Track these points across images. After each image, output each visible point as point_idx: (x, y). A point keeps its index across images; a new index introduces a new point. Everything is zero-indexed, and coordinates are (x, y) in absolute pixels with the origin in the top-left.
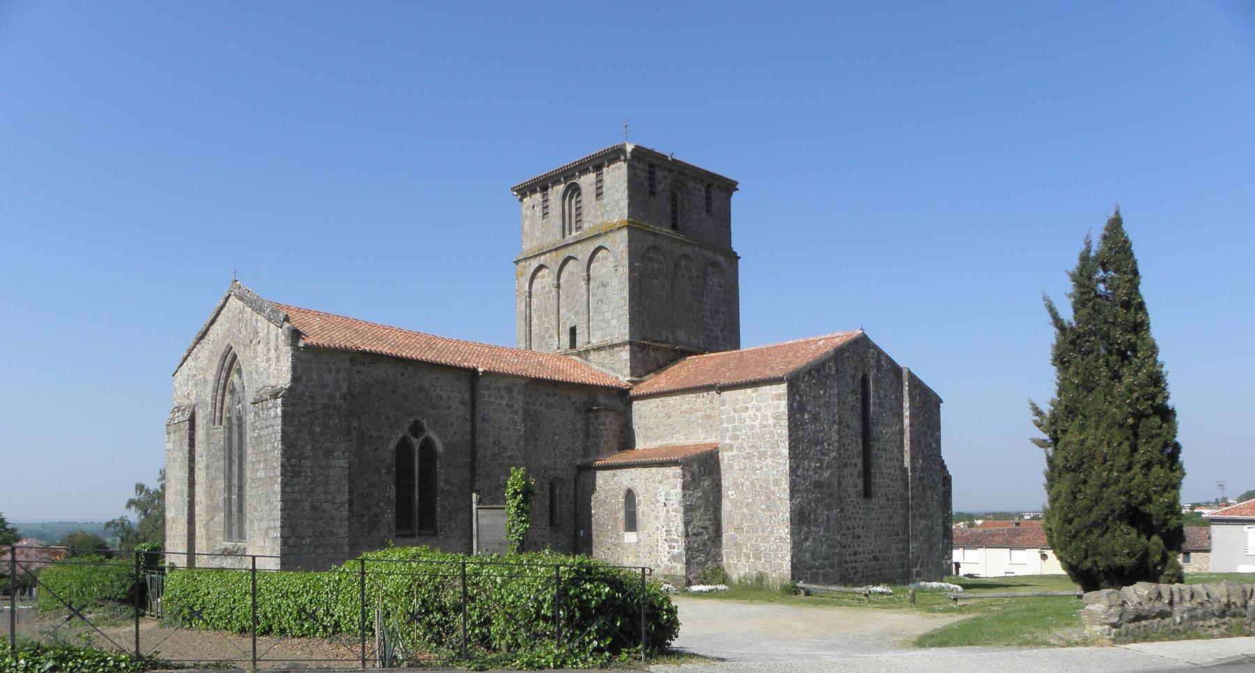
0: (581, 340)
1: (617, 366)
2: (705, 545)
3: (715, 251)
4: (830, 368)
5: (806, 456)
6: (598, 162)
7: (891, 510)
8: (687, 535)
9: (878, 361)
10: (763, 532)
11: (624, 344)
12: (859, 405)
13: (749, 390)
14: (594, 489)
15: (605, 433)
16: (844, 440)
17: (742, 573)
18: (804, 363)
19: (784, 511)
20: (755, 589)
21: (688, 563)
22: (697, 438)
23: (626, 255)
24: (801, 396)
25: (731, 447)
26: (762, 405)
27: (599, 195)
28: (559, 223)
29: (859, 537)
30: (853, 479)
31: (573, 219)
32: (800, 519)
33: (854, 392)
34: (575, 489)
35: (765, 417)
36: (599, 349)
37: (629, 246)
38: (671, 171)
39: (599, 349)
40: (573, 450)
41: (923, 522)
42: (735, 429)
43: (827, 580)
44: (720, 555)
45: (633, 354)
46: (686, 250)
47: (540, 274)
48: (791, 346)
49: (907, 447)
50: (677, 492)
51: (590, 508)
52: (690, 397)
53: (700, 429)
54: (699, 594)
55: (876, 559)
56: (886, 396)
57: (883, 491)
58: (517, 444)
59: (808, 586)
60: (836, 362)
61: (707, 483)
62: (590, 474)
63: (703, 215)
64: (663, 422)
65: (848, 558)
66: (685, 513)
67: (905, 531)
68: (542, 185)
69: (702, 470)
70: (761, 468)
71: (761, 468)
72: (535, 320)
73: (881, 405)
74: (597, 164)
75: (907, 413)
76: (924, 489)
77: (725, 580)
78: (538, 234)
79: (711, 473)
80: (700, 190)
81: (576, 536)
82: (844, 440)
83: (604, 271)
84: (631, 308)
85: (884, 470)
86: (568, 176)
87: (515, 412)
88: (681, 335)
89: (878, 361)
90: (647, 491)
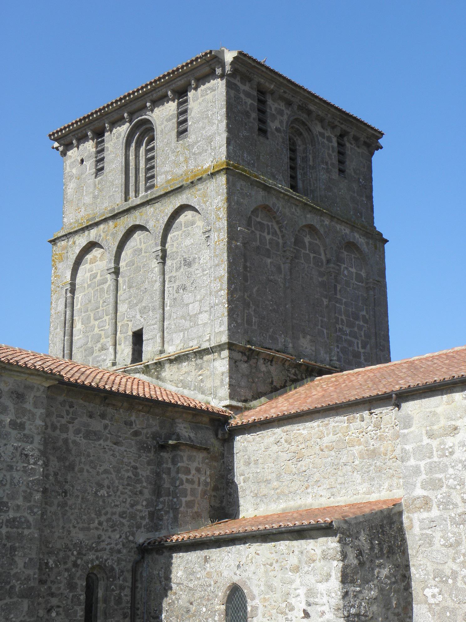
0: (150, 351)
1: (208, 384)
3: (353, 227)
6: (180, 83)
11: (220, 348)
14: (166, 588)
15: (188, 486)
22: (358, 492)
23: (223, 214)
25: (426, 503)
27: (182, 132)
28: (120, 180)
31: (142, 175)
34: (134, 589)
36: (178, 359)
37: (229, 199)
38: (289, 104)
39: (178, 359)
40: (133, 517)
42: (431, 469)
45: (233, 363)
46: (311, 219)
47: (89, 257)
52: (337, 422)
53: (357, 477)
58: (28, 498)
61: (385, 572)
62: (162, 560)
63: (335, 175)
64: (288, 466)
68: (93, 128)
72: (78, 326)
74: (178, 86)
78: (88, 199)
79: (391, 551)
80: (329, 139)
83: (188, 242)
84: (231, 293)
86: (132, 112)
87: (28, 439)
90: (270, 588)
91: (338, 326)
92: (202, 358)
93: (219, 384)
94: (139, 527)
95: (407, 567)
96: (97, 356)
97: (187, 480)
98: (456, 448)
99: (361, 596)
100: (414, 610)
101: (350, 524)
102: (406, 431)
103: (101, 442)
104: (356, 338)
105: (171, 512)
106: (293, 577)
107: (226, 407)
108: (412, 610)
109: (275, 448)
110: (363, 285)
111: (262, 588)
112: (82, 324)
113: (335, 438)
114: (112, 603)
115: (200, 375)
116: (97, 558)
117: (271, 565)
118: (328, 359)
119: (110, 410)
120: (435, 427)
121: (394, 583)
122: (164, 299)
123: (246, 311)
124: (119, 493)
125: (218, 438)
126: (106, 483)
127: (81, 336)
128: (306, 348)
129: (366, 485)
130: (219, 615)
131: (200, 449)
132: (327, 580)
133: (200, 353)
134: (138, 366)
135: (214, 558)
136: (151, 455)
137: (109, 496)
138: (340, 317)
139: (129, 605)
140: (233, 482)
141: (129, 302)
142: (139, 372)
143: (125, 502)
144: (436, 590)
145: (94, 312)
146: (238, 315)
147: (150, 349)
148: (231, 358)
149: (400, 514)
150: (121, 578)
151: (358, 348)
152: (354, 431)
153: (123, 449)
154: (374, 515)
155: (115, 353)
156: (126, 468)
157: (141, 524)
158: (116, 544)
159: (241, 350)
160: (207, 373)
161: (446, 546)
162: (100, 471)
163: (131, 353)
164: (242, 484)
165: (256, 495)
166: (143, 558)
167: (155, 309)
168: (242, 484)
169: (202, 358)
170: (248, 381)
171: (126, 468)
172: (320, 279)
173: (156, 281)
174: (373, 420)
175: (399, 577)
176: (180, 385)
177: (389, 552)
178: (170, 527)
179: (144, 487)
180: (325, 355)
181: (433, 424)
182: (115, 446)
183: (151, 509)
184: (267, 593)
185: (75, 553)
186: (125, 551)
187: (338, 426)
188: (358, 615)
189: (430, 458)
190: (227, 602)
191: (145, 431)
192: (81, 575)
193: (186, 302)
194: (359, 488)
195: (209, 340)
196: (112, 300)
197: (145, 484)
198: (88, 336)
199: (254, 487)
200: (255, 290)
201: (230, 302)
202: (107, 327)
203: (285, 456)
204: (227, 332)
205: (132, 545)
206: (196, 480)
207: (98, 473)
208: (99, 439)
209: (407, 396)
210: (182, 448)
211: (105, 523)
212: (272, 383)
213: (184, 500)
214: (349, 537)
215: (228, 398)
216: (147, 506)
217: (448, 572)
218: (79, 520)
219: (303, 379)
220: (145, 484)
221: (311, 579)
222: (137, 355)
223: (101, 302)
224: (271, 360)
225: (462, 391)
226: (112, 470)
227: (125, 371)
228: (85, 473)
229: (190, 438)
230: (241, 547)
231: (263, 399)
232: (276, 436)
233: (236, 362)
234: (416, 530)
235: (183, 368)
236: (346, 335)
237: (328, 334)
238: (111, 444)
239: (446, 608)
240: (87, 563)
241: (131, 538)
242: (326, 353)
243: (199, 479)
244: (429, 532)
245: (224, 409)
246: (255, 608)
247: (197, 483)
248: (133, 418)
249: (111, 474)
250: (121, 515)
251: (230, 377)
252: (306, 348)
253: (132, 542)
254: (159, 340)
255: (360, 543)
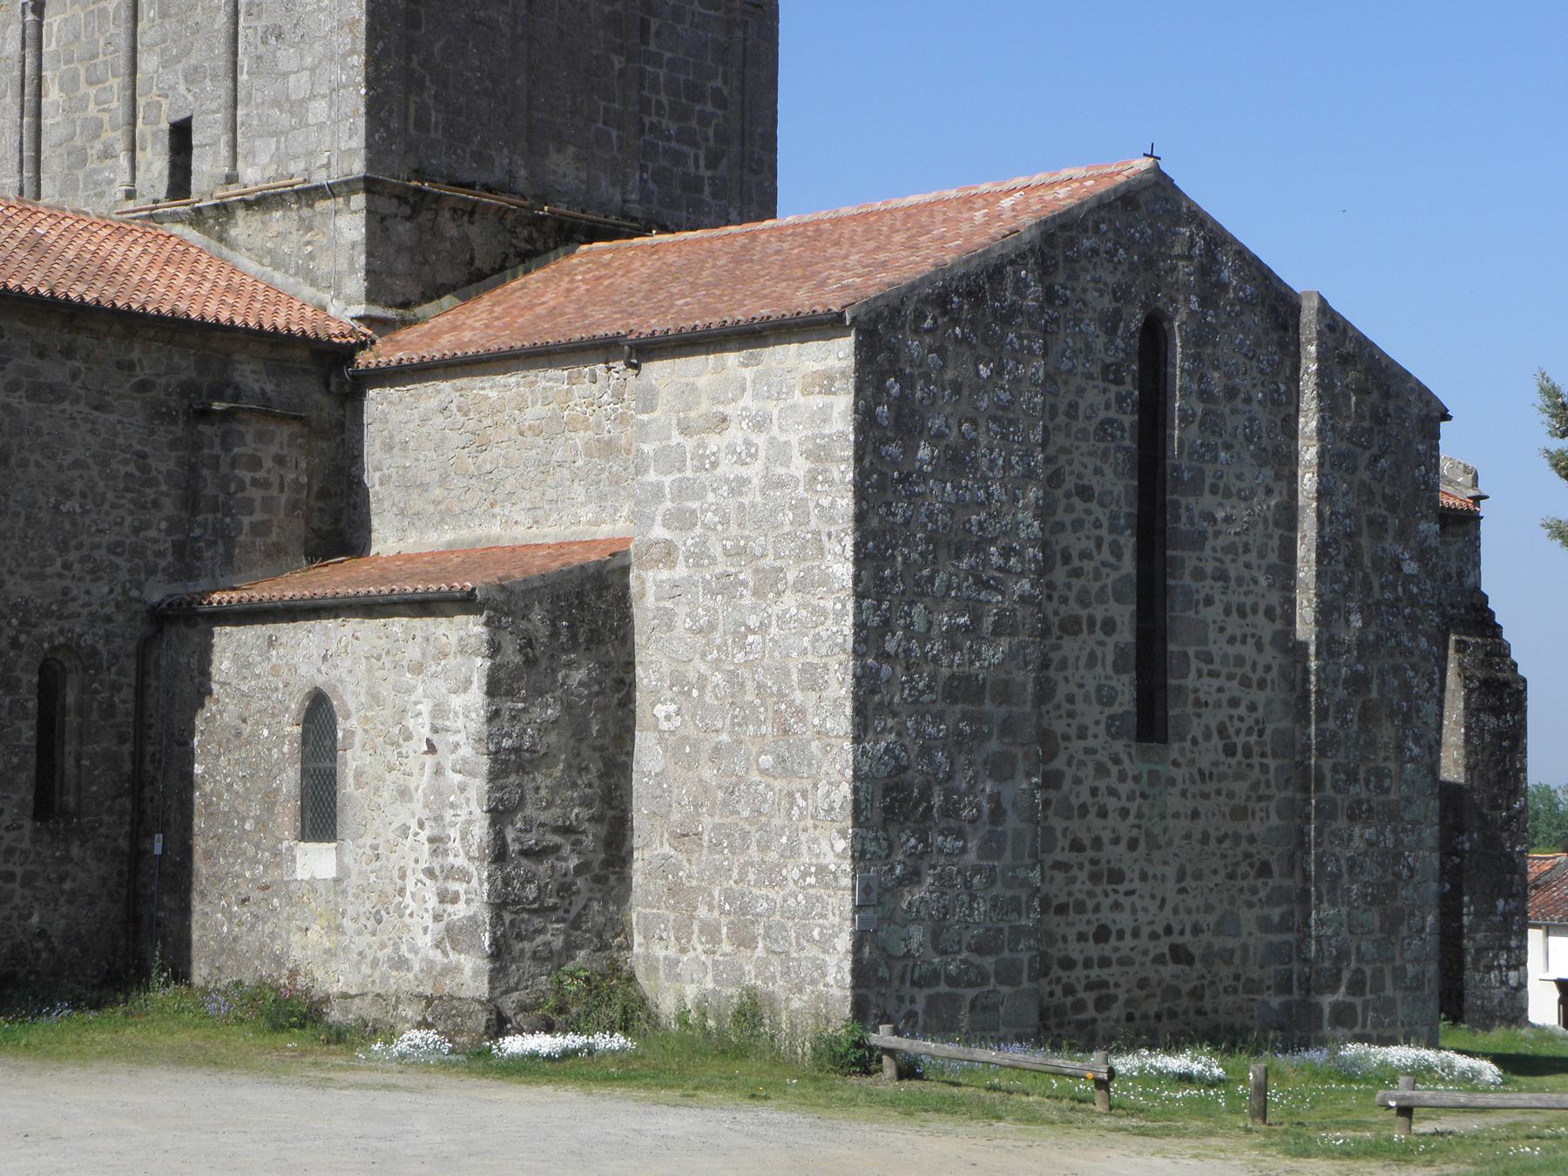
0: (206, 167)
1: (324, 265)
2: (565, 889)
4: (1020, 287)
5: (919, 591)
7: (1241, 788)
8: (499, 855)
9: (1208, 268)
10: (764, 847)
12: (1129, 420)
13: (732, 358)
14: (202, 692)
15: (256, 494)
16: (1067, 539)
17: (691, 992)
18: (927, 268)
19: (835, 784)
20: (729, 1053)
21: (499, 953)
24: (907, 382)
25: (668, 553)
26: (773, 408)
29: (1117, 877)
30: (1098, 677)
32: (890, 808)
33: (1111, 373)
34: (140, 690)
35: (780, 453)
36: (262, 202)
39: (262, 202)
41: (1361, 834)
42: (684, 490)
43: (987, 1029)
44: (620, 927)
45: (377, 224)
48: (909, 213)
49: (1306, 571)
50: (469, 705)
51: (188, 758)
52: (551, 380)
53: (579, 491)
54: (529, 1068)
55: (1180, 955)
56: (1231, 393)
57: (1212, 718)
59: (904, 1044)
60: (1045, 267)
61: (579, 675)
64: (463, 466)
65: (1075, 950)
66: (494, 776)
67: (1292, 863)
69: (566, 637)
70: (763, 627)
71: (763, 627)
72: (53, 95)
73: (1211, 423)
75: (1309, 453)
76: (1366, 716)
77: (631, 1014)
79: (595, 638)
81: (137, 854)
82: (1067, 539)
84: (374, 61)
85: (1218, 646)
88: (563, 167)
89: (1208, 268)
90: (375, 698)
91: (647, 120)
92: (311, 206)
93: (346, 266)
94: (151, 571)
95: (630, 665)
96: (95, 171)
97: (255, 482)
98: (722, 455)
99: (525, 718)
100: (637, 740)
101: (512, 592)
102: (645, 417)
103: (66, 405)
104: (695, 144)
105: (220, 542)
106: (413, 682)
107: (359, 319)
108: (633, 740)
109: (439, 420)
110: (720, 13)
111: (363, 699)
112: (61, 90)
113: (545, 411)
114: (95, 716)
115: (308, 243)
116: (61, 632)
117: (379, 658)
118: (618, 197)
119: (83, 340)
120: (692, 414)
121: (597, 694)
122: (235, 54)
123: (413, 98)
124: (106, 506)
125: (329, 392)
126: (78, 486)
127: (59, 118)
128: (564, 176)
129: (593, 506)
130: (291, 744)
131: (283, 418)
132: (466, 690)
133: (309, 194)
134: (181, 208)
135: (284, 640)
136: (178, 430)
137: (85, 512)
138: (654, 97)
139: (131, 719)
140: (361, 483)
141: (163, 51)
142: (182, 221)
143: (121, 524)
144: (673, 708)
145: (87, 64)
146: (391, 111)
147: (206, 167)
148: (371, 212)
149: (625, 570)
150: (113, 670)
151: (697, 167)
152: (578, 400)
153: (114, 418)
154: (565, 575)
155: (134, 168)
156: (122, 456)
157: (156, 565)
158: (102, 606)
159: (397, 192)
160: (322, 240)
161: (693, 632)
162: (65, 463)
163: (166, 173)
164: (377, 487)
165: (402, 512)
166: (160, 631)
167: (216, 75)
168: (377, 487)
169: (311, 206)
170: (413, 261)
171: (122, 456)
172: (607, 9)
173: (219, 8)
174: (612, 382)
175: (608, 683)
176: (267, 261)
177: (589, 641)
178: (218, 573)
179: (163, 494)
180: (611, 191)
181: (688, 408)
182: (96, 413)
183: (180, 537)
184: (371, 708)
185: (14, 622)
186: (121, 618)
187: (552, 388)
188: (517, 750)
189: (680, 470)
190: (305, 721)
191: (163, 381)
192: (27, 664)
193: (283, 66)
194: (581, 512)
195: (328, 166)
196: (123, 42)
197: (164, 488)
198: (74, 121)
199: (398, 496)
200: (437, 48)
201: (370, 83)
202: (115, 104)
203: (455, 439)
204: (363, 152)
205: (138, 606)
206: (274, 479)
207: (60, 468)
208: (61, 400)
209: (652, 351)
210: (242, 416)
211: (77, 566)
212: (471, 262)
213: (246, 520)
214: (507, 615)
215: (363, 299)
216: (168, 531)
217: (692, 676)
218: (21, 560)
219: (547, 250)
220: (164, 488)
221: (440, 686)
222: (180, 182)
223: (102, 43)
224: (471, 212)
225: (739, 350)
226: (90, 461)
227: (151, 217)
228: (33, 470)
229: (263, 393)
230: (330, 624)
231: (447, 300)
232: (442, 396)
233: (383, 219)
234: (650, 601)
235: (274, 223)
236: (669, 138)
237: (620, 138)
238: (88, 410)
239: (685, 739)
240: (40, 641)
241: (134, 593)
242: (614, 185)
243: (282, 477)
244: (669, 604)
245: (355, 324)
246: (350, 734)
247: (276, 486)
248: (135, 355)
249: (89, 468)
250: (113, 549)
251: (369, 255)
252: (564, 176)
253: (138, 600)
254: (224, 151)
255: (530, 626)
